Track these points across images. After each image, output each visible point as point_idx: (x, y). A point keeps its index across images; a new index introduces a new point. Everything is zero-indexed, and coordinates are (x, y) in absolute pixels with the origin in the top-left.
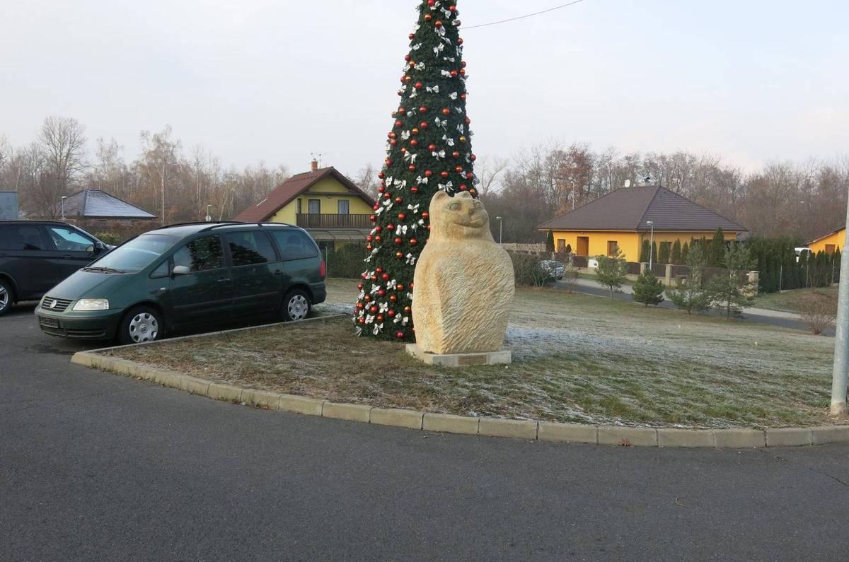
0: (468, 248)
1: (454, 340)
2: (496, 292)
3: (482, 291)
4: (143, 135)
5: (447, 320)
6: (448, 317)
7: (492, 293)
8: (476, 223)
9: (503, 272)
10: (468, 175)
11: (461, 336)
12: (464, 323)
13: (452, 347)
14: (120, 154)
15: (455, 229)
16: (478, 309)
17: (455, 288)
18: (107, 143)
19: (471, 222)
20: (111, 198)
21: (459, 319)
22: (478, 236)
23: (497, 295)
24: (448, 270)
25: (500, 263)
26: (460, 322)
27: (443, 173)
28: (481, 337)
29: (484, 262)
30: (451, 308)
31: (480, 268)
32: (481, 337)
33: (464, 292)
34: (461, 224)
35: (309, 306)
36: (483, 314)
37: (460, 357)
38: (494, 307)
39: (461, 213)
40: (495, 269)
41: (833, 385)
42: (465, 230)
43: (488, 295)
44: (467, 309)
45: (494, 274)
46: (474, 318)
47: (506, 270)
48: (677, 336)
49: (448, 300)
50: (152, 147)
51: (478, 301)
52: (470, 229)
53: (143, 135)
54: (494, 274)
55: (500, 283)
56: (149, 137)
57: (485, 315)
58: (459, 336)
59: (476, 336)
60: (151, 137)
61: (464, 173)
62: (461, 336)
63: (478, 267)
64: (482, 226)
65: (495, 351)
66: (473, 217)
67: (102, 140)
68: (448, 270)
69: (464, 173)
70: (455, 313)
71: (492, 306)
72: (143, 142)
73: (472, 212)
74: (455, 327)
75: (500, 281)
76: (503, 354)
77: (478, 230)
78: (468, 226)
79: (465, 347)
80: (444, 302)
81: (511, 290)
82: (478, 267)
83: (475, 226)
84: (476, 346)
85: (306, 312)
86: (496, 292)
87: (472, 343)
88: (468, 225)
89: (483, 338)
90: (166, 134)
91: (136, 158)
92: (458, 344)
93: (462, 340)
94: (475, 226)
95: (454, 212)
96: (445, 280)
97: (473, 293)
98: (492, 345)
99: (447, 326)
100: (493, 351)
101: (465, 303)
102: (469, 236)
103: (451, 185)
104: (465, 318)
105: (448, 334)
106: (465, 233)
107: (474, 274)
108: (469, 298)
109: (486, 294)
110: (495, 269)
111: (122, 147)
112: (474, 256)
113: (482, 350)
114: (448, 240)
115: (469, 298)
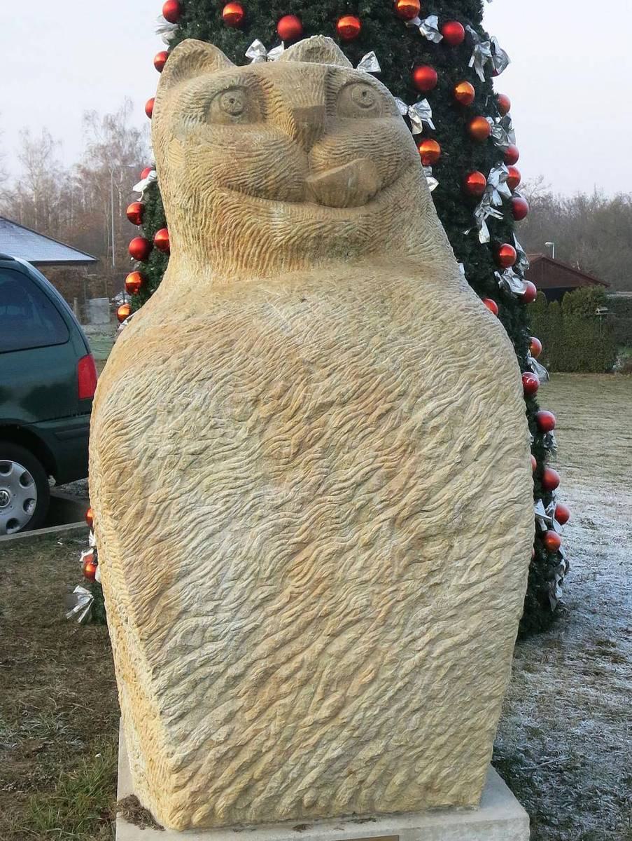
0: (281, 313)
1: (227, 773)
2: (424, 539)
3: (351, 536)
4: (86, 118)
5: (172, 684)
6: (179, 665)
7: (401, 540)
8: (331, 185)
9: (463, 434)
10: (449, 29)
11: (258, 755)
12: (267, 692)
13: (222, 803)
14: (56, 154)
15: (230, 218)
16: (330, 626)
17: (199, 522)
18: (36, 137)
19: (312, 179)
20: (20, 230)
21: (237, 678)
22: (358, 247)
23: (432, 549)
24: (165, 427)
25: (448, 384)
26: (243, 686)
27: (342, 24)
28: (367, 753)
29: (351, 385)
30: (190, 622)
31: (333, 418)
32: (367, 753)
33: (251, 542)
34: (258, 192)
35: (42, 489)
36: (361, 648)
38: (423, 612)
39: (256, 136)
40: (419, 415)
42: (282, 219)
43: (384, 551)
44: (276, 624)
45: (409, 448)
46: (314, 665)
47: (479, 418)
49: (167, 582)
50: (103, 138)
51: (328, 584)
52: (309, 215)
53: (86, 118)
54: (409, 448)
55: (447, 492)
56: (97, 122)
58: (246, 756)
59: (335, 750)
60: (100, 122)
61: (433, 21)
62: (258, 755)
63: (323, 408)
64: (371, 199)
65: (450, 809)
66: (320, 153)
67: (27, 133)
68: (165, 427)
69: (433, 21)
70: (210, 648)
71: (412, 607)
72: (86, 132)
73: (311, 130)
74: (221, 712)
75: (453, 475)
76: (488, 825)
77: (351, 219)
78: (299, 199)
79: (287, 801)
80: (147, 593)
81: (508, 526)
82: (323, 408)
83: (333, 196)
84: (344, 795)
85: (31, 508)
86: (424, 539)
87: (321, 783)
88: (297, 195)
89: (373, 760)
90: (125, 114)
91: (79, 160)
92: (246, 790)
93: (266, 774)
94: (333, 196)
95: (221, 132)
96: (146, 482)
97: (303, 545)
98: (428, 787)
99: (176, 708)
100: (437, 810)
101: (259, 594)
102: (300, 250)
103: (376, 67)
104: (267, 674)
107: (301, 447)
108: (281, 572)
109: (371, 550)
110: (419, 415)
111: (60, 142)
112: (304, 354)
113: (380, 808)
114: (208, 275)
115: (281, 572)
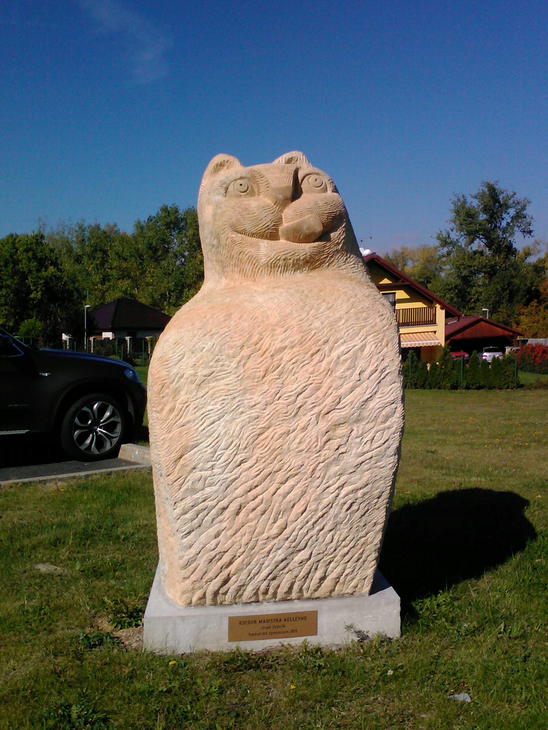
2: (338, 425)
3: (293, 425)
6: (189, 501)
7: (323, 425)
9: (361, 364)
16: (279, 477)
30: (197, 474)
31: (286, 356)
33: (235, 427)
36: (296, 491)
37: (232, 620)
39: (253, 203)
40: (334, 354)
41: (430, 390)
42: (265, 249)
43: (313, 432)
44: (247, 475)
45: (329, 371)
48: (308, 447)
57: (304, 493)
58: (226, 558)
74: (212, 531)
86: (338, 425)
96: (177, 392)
101: (239, 458)
105: (193, 551)
106: (264, 260)
110: (334, 354)
